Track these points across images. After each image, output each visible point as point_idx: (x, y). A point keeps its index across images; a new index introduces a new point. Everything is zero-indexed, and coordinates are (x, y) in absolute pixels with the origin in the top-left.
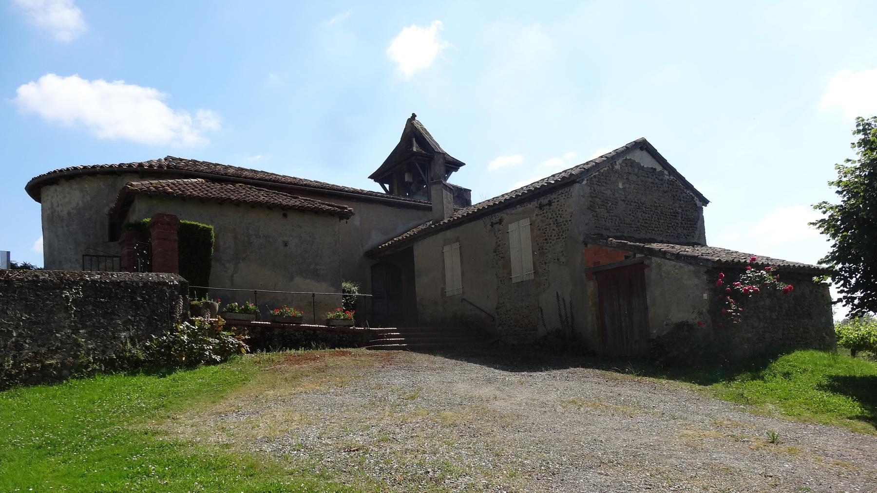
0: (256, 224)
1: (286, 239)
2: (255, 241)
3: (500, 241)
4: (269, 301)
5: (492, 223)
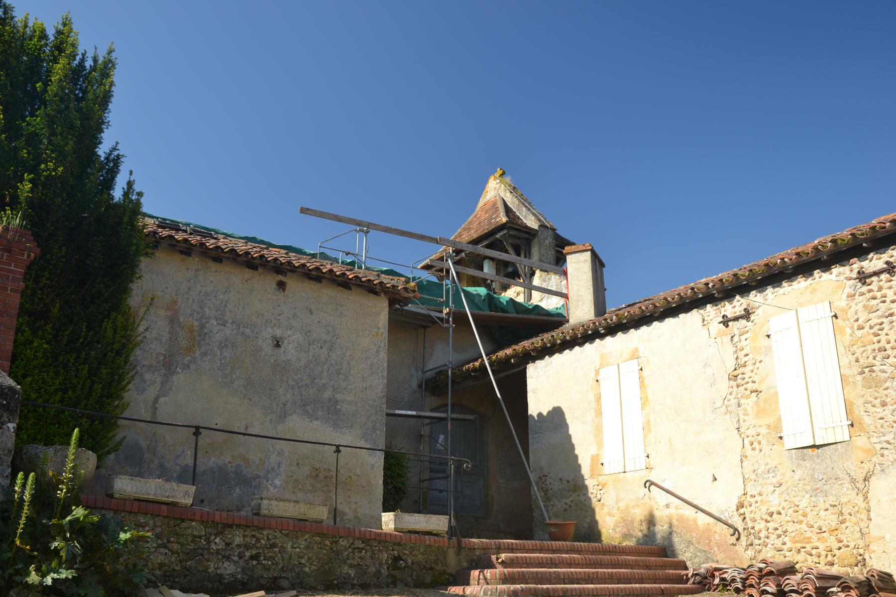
0: (221, 297)
1: (278, 333)
2: (215, 331)
3: (746, 355)
4: (229, 462)
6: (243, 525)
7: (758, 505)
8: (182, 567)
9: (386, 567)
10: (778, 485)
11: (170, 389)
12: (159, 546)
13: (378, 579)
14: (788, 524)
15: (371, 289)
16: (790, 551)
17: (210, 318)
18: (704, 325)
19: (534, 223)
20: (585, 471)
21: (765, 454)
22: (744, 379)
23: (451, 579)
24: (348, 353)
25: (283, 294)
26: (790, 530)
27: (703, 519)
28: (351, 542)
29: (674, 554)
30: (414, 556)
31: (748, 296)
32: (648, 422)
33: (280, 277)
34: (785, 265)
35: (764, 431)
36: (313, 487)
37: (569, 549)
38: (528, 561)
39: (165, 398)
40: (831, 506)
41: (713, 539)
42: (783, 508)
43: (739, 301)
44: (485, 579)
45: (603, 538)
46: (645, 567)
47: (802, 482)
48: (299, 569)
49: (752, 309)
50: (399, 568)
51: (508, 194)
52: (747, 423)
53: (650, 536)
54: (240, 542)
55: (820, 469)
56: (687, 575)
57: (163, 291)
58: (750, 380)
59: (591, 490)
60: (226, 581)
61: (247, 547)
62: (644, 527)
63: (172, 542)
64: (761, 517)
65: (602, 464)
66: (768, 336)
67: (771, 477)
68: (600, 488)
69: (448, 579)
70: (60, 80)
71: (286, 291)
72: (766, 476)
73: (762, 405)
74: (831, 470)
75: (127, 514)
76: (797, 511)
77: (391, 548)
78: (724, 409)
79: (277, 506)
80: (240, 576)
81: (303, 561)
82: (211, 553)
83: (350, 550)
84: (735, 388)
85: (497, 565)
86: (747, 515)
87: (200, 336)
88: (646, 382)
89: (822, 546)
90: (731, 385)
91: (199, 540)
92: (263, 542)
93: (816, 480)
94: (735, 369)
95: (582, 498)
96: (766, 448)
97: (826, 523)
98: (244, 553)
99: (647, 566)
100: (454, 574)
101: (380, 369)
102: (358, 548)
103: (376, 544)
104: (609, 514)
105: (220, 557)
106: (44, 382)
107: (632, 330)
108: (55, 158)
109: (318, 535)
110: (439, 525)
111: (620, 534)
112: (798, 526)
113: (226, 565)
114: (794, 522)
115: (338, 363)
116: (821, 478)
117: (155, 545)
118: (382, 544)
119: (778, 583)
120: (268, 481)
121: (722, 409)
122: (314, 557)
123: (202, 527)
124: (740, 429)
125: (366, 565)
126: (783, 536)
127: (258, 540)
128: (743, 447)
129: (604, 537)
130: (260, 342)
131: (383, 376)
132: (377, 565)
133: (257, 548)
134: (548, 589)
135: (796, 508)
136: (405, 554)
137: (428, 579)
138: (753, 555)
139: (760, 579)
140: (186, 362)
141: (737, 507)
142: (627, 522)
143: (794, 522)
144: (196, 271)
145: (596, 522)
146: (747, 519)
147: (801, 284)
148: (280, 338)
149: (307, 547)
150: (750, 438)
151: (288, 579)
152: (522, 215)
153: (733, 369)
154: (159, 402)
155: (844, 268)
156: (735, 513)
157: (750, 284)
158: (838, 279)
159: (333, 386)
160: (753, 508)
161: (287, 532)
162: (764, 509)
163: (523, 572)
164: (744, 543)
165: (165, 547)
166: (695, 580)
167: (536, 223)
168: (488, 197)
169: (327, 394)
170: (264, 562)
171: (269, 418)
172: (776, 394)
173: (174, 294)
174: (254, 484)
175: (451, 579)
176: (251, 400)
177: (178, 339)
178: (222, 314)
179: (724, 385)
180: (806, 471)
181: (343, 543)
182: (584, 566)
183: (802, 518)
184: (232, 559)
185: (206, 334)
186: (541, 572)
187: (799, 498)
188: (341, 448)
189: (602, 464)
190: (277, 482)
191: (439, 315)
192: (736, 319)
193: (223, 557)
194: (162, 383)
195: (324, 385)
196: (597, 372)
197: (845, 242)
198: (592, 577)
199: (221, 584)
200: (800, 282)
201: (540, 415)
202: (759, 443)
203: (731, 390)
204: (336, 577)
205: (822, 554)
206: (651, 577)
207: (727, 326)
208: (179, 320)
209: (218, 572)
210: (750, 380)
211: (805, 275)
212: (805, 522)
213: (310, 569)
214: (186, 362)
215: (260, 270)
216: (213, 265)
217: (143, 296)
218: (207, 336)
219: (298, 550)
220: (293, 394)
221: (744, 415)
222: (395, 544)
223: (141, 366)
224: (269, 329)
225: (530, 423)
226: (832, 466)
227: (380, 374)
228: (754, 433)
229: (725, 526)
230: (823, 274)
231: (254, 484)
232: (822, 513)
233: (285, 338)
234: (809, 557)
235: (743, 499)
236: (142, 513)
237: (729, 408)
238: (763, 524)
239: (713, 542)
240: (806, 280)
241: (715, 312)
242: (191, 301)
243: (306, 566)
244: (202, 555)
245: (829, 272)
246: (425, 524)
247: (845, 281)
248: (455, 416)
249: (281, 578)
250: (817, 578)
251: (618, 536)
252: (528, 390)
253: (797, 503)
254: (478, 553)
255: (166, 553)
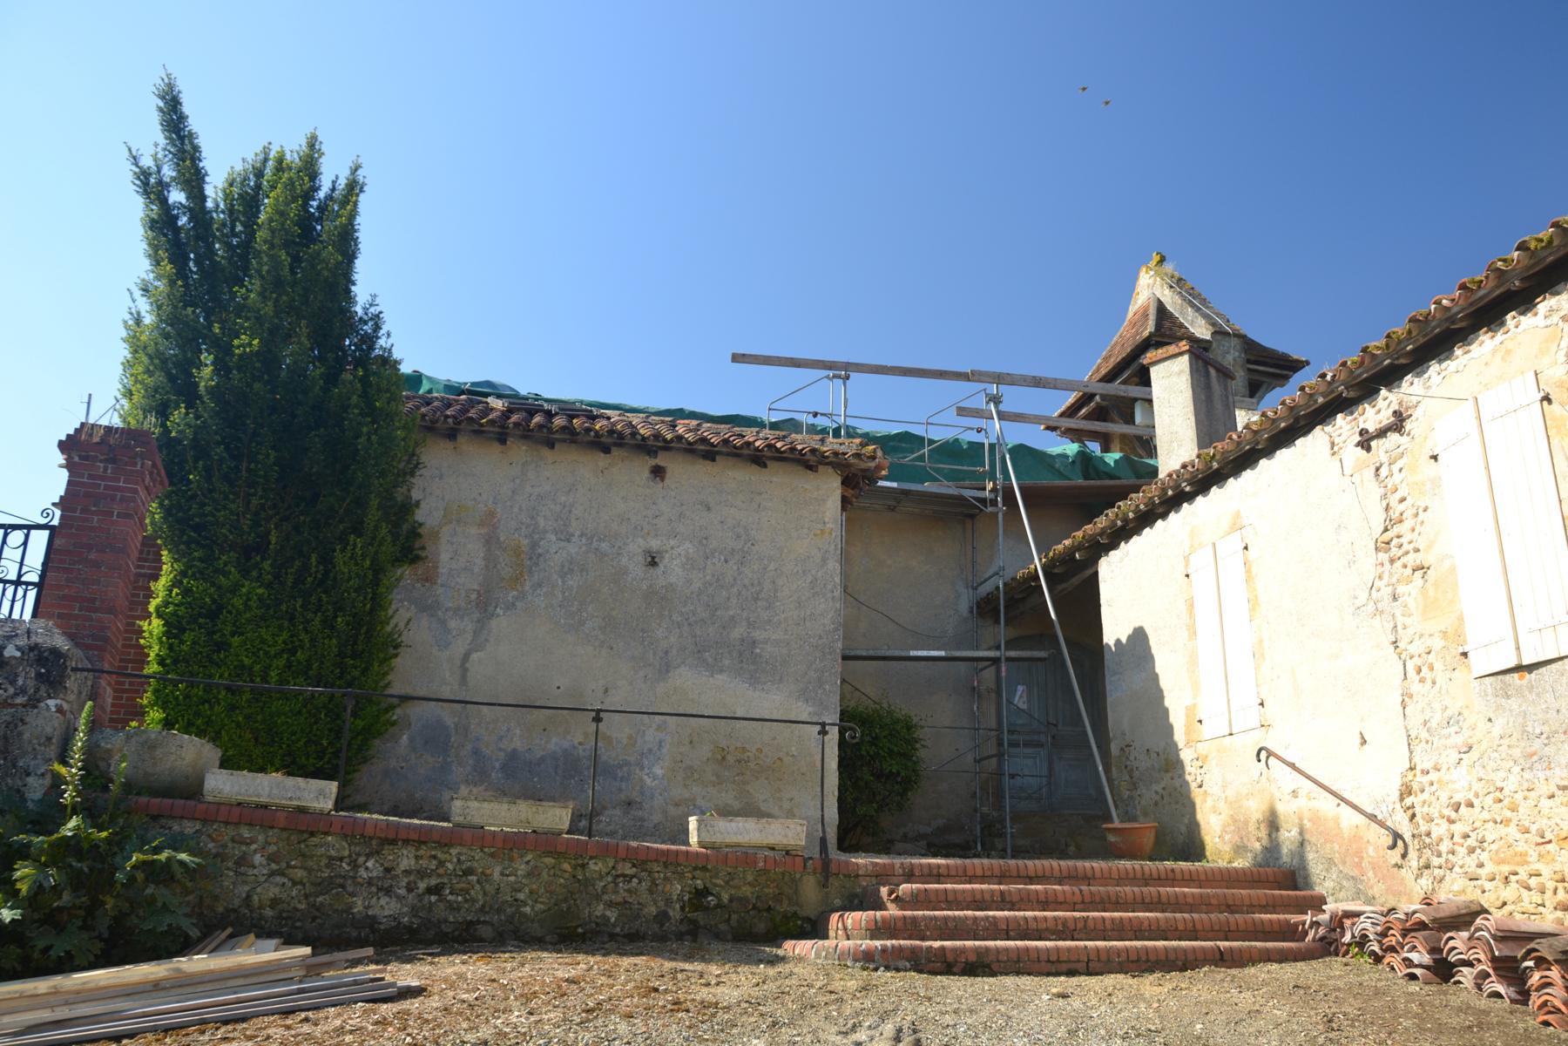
1: (654, 544)
3: (1403, 500)
4: (580, 744)
5: (1363, 432)
6: (414, 841)
7: (1433, 788)
8: (308, 904)
9: (678, 906)
10: (1465, 749)
11: (487, 640)
12: (272, 874)
13: (662, 925)
14: (1486, 825)
15: (809, 462)
16: (1491, 880)
17: (546, 532)
18: (1333, 454)
19: (1204, 330)
20: (1179, 736)
21: (1441, 688)
22: (1400, 546)
23: (808, 927)
24: (772, 567)
25: (661, 485)
26: (1489, 838)
27: (1349, 819)
28: (611, 865)
29: (1308, 885)
30: (735, 887)
31: (1399, 387)
32: (1261, 641)
33: (653, 462)
34: (1448, 314)
35: (1437, 643)
36: (718, 776)
37: (1065, 874)
38: (950, 898)
39: (479, 653)
40: (1559, 788)
41: (1365, 855)
42: (1477, 796)
43: (1385, 399)
44: (845, 929)
45: (1208, 854)
46: (1223, 908)
47: (1506, 742)
48: (513, 909)
49: (1407, 410)
50: (707, 909)
51: (1167, 291)
52: (1410, 631)
53: (1272, 849)
54: (410, 866)
55: (1535, 714)
56: (1304, 923)
57: (475, 499)
58: (1412, 546)
59: (1188, 769)
60: (382, 927)
61: (422, 874)
62: (1263, 833)
63: (294, 867)
64: (1440, 812)
65: (1200, 721)
66: (1435, 458)
67: (1453, 734)
68: (1200, 764)
69: (802, 927)
70: (271, 220)
71: (667, 481)
72: (1445, 731)
73: (1431, 593)
74: (1555, 713)
75: (222, 825)
76: (1500, 801)
77: (690, 875)
78: (1370, 608)
79: (479, 809)
80: (406, 919)
81: (521, 896)
82: (359, 883)
83: (610, 879)
84: (1387, 565)
85: (889, 905)
86: (1418, 810)
87: (530, 559)
88: (1254, 570)
89: (1546, 871)
90: (1380, 561)
91: (338, 863)
92: (450, 866)
93: (1531, 736)
94: (1386, 530)
95: (1177, 783)
96: (1441, 676)
97: (1552, 823)
98: (415, 883)
99: (1228, 906)
100: (813, 917)
101: (829, 587)
102: (624, 876)
103: (659, 869)
104: (1214, 810)
105: (374, 889)
106: (263, 641)
107: (1231, 480)
108: (250, 328)
109: (549, 854)
110: (786, 836)
111: (1230, 846)
112: (1502, 830)
113: (383, 901)
114: (1496, 823)
115: (756, 582)
116: (1538, 731)
117: (265, 872)
118: (672, 868)
119: (1436, 945)
120: (642, 768)
121: (1369, 607)
122: (542, 890)
123: (344, 843)
124: (1398, 644)
125: (639, 904)
126: (1478, 851)
127: (441, 863)
128: (1405, 678)
129: (1209, 851)
130: (624, 561)
131: (833, 597)
132: (661, 904)
133: (439, 876)
134: (943, 949)
135: (1498, 794)
136: (716, 885)
137: (761, 927)
138: (1430, 888)
139: (1404, 936)
140: (510, 598)
141: (1401, 795)
142: (1238, 823)
143: (1496, 823)
144: (523, 465)
145: (1197, 825)
146: (1418, 818)
147: (1485, 345)
148: (658, 552)
149: (529, 874)
150: (1415, 659)
151: (493, 925)
152: (1187, 321)
153: (1382, 529)
154: (471, 659)
155: (1557, 297)
156: (1398, 806)
157: (1396, 362)
158: (1549, 322)
159: (748, 619)
160: (1426, 796)
161: (493, 850)
162: (1444, 797)
163: (914, 918)
164: (1414, 864)
165: (283, 875)
166: (1316, 932)
167: (1207, 329)
168: (1140, 302)
169: (737, 632)
170: (450, 897)
171: (641, 673)
172: (1453, 569)
173: (490, 502)
174: (620, 774)
175: (808, 927)
176: (612, 648)
177: (499, 566)
178: (565, 525)
179: (1368, 561)
180: (1512, 719)
181: (595, 867)
182: (1077, 907)
183: (1508, 814)
184: (395, 892)
185: (540, 555)
186: (954, 918)
187: (1502, 774)
188: (602, 715)
189: (1200, 721)
190: (658, 771)
191: (979, 494)
192: (1382, 433)
193: (380, 889)
194: (475, 632)
195: (732, 618)
196: (1187, 559)
197: (1543, 244)
198: (1072, 927)
199: (373, 931)
200: (1483, 342)
201: (1118, 642)
202: (1431, 668)
203: (1380, 569)
204: (579, 923)
205: (1547, 886)
206: (1217, 928)
207: (1369, 449)
208: (498, 539)
209: (370, 913)
210: (1412, 546)
211: (1492, 326)
212: (1515, 822)
213: (533, 909)
214: (510, 598)
215: (615, 452)
216: (546, 452)
217: (445, 509)
218: (541, 559)
219: (512, 878)
220: (681, 636)
221: (1404, 615)
222: (695, 869)
223: (444, 610)
224: (640, 540)
225: (1108, 659)
226: (1557, 705)
227: (829, 595)
228: (1422, 650)
229: (1383, 831)
230: (1522, 318)
231: (620, 774)
232: (1545, 803)
233: (667, 551)
234: (1525, 893)
235: (1410, 778)
236: (246, 824)
237: (1379, 605)
238: (1444, 824)
239: (1366, 860)
240: (1493, 337)
241: (1349, 427)
242: (516, 510)
243: (525, 904)
244: (343, 886)
245: (1533, 312)
246: (758, 835)
247: (1561, 324)
248: (1012, 654)
249: (479, 922)
250: (1495, 937)
251: (1227, 848)
252: (1103, 601)
253: (1499, 785)
254: (864, 884)
255: (284, 884)
